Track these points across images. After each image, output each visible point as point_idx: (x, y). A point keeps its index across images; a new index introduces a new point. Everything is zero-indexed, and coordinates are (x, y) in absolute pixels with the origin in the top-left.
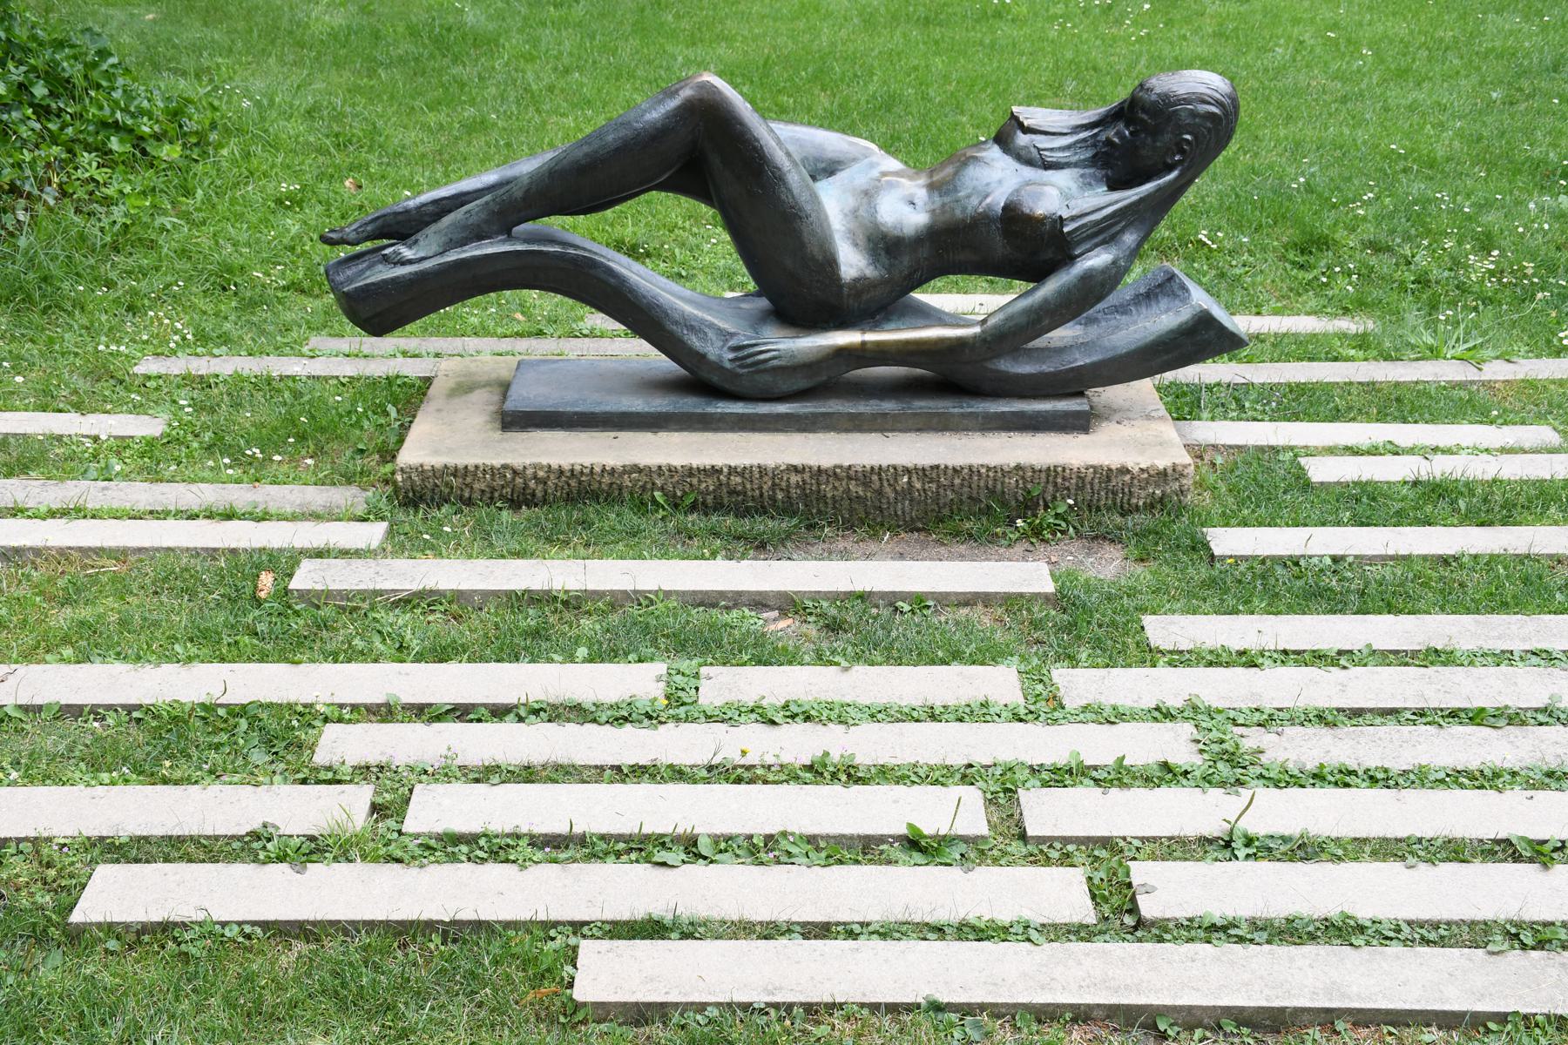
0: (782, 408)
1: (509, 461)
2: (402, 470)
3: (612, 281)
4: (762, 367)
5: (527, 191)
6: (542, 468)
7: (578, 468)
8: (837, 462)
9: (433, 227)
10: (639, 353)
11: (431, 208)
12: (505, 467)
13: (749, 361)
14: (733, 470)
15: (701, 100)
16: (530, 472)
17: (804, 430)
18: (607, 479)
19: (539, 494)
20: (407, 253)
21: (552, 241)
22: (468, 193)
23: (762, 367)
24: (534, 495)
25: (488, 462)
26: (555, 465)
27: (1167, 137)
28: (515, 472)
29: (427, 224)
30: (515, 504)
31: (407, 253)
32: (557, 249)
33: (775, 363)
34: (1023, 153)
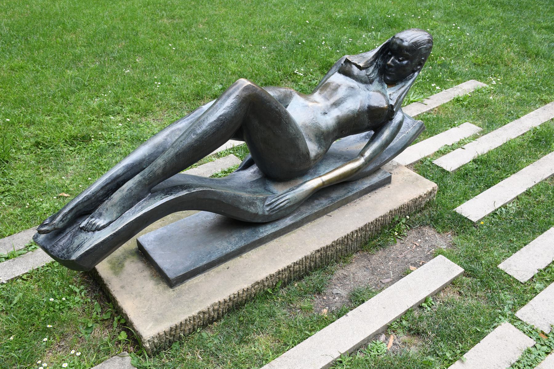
0: (288, 221)
1: (200, 309)
2: (149, 341)
3: (215, 198)
4: (282, 208)
5: (164, 169)
6: (216, 304)
7: (232, 296)
8: (333, 240)
9: (108, 204)
10: (205, 217)
11: (102, 192)
12: (199, 313)
13: (277, 207)
14: (295, 264)
15: (249, 96)
16: (211, 309)
17: (299, 227)
18: (245, 294)
19: (216, 316)
20: (101, 222)
21: (182, 187)
22: (118, 177)
23: (282, 208)
24: (213, 318)
25: (191, 315)
26: (222, 301)
27: (417, 60)
28: (204, 313)
29: (102, 201)
30: (204, 326)
31: (101, 222)
32: (184, 193)
33: (288, 205)
34: (363, 79)
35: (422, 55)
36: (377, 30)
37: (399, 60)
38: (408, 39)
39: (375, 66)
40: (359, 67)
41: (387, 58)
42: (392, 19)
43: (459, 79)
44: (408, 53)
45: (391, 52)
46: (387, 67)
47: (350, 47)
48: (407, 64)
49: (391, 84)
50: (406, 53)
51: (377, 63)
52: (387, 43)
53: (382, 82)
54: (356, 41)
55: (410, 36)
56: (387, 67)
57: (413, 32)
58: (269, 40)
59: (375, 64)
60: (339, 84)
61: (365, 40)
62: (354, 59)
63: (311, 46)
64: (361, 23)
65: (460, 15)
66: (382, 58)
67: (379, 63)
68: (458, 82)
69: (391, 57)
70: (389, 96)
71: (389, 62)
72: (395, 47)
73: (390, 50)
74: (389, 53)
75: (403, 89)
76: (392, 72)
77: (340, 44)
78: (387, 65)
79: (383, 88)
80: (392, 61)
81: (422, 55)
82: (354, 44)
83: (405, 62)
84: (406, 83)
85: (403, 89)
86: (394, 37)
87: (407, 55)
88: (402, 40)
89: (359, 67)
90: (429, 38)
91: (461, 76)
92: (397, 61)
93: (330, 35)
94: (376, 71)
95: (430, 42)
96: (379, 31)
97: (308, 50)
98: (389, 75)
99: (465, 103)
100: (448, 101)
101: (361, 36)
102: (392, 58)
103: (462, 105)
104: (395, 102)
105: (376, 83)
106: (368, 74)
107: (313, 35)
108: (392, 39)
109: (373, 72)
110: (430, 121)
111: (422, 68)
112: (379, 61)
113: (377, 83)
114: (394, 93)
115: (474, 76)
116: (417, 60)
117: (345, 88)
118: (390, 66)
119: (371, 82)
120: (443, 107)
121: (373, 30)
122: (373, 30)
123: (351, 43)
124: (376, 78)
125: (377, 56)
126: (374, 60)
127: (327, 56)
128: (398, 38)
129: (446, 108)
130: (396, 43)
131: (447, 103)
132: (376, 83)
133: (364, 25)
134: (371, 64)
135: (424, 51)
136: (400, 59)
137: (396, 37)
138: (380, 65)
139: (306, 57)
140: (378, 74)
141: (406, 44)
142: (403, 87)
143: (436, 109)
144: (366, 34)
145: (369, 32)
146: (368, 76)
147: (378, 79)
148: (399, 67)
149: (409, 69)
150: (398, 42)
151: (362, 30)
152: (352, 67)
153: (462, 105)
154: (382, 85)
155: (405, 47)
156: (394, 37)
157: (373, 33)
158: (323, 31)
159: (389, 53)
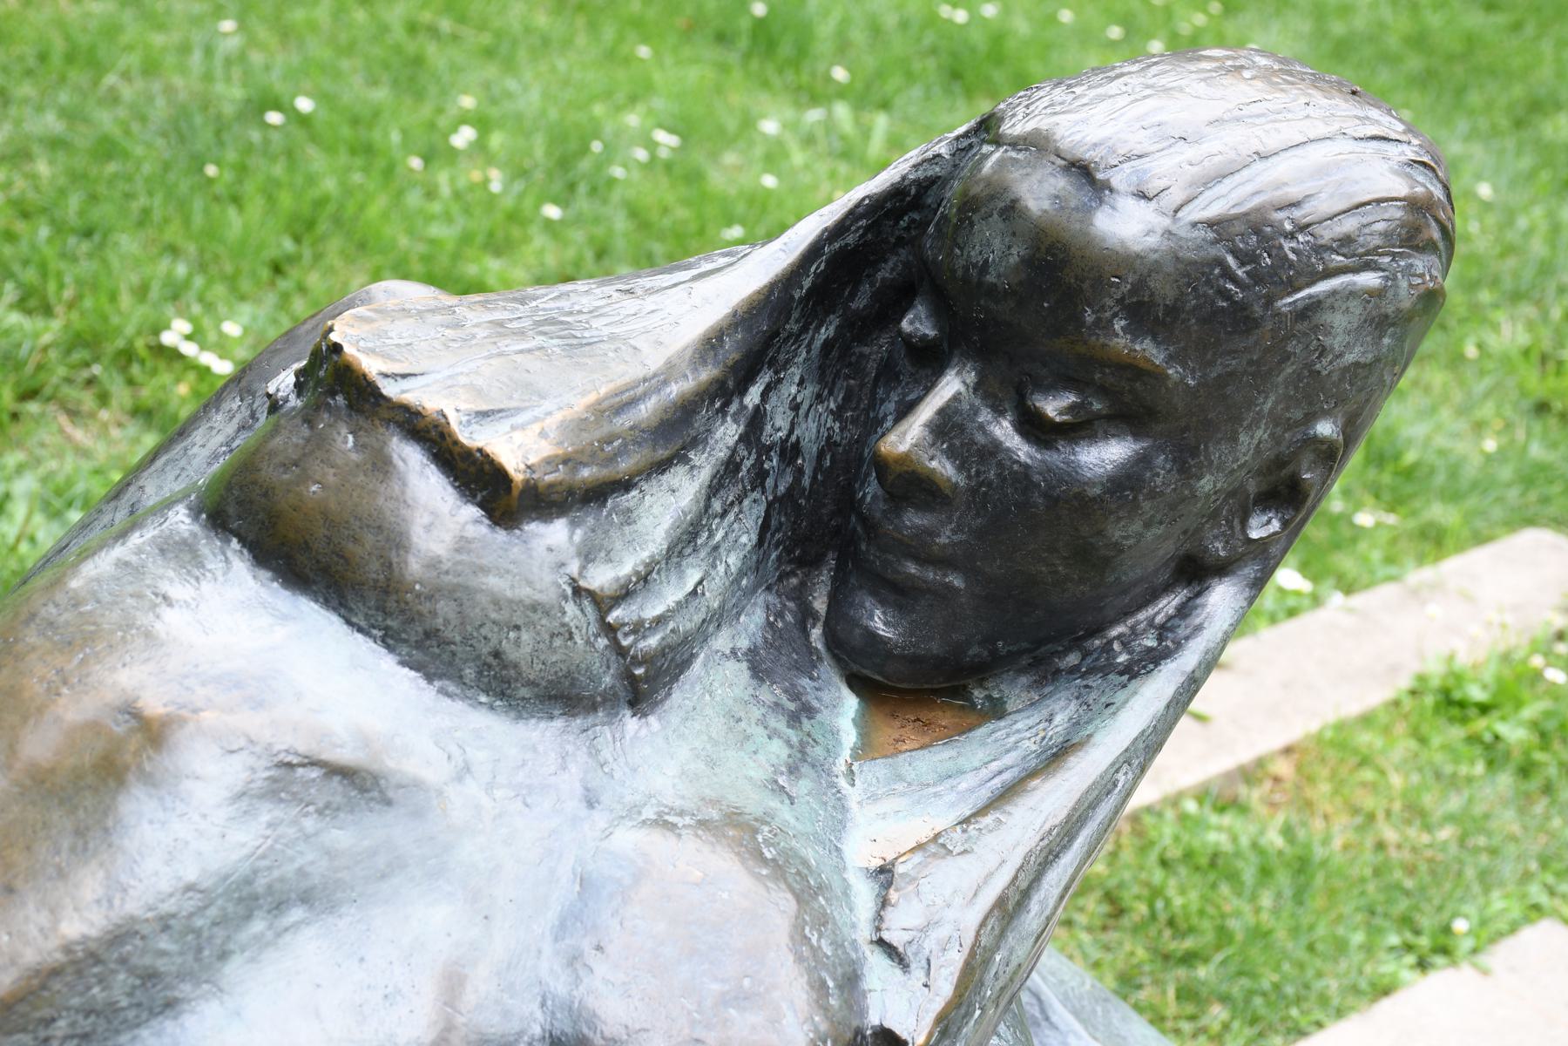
27: (1252, 442)
34: (522, 648)
35: (1313, 392)
36: (866, 97)
37: (1034, 427)
38: (1170, 169)
39: (730, 467)
40: (477, 477)
41: (888, 374)
42: (978, 38)
43: (1440, 513)
44: (1150, 351)
45: (942, 310)
46: (871, 489)
47: (659, 193)
48: (1125, 482)
49: (921, 688)
50: (1121, 341)
51: (756, 420)
52: (897, 193)
53: (807, 663)
54: (714, 156)
55: (1179, 145)
56: (871, 489)
57: (1239, 91)
58: (43, 57)
59: (728, 433)
60: (154, 704)
61: (774, 157)
62: (402, 338)
63: (365, 150)
64: (764, 38)
65: (1415, 63)
66: (831, 368)
67: (779, 423)
68: (1434, 542)
69: (928, 361)
70: (864, 895)
71: (906, 438)
72: (994, 250)
73: (915, 281)
74: (917, 323)
75: (1053, 798)
76: (926, 559)
77: (585, 165)
78: (881, 465)
79: (801, 760)
80: (947, 427)
81: (1313, 392)
82: (694, 177)
83: (1105, 455)
84: (1097, 710)
85: (1053, 798)
86: (987, 128)
87: (1135, 371)
88: (1082, 171)
89: (477, 477)
90: (1426, 186)
91: (1452, 495)
92: (1004, 432)
93: (529, 92)
94: (739, 534)
95: (1424, 227)
96: (885, 105)
97: (327, 175)
98: (899, 594)
99: (1514, 733)
100: (1375, 697)
101: (748, 123)
102: (950, 386)
103: (1494, 753)
104: (945, 987)
105: (718, 684)
106: (601, 578)
107: (410, 75)
108: (963, 149)
109: (687, 539)
110: (1233, 877)
111: (1291, 531)
112: (791, 405)
113: (737, 672)
114: (933, 847)
115: (1545, 500)
116: (1252, 442)
117: (236, 771)
118: (910, 486)
119: (642, 684)
120: (1336, 752)
121: (842, 92)
122: (842, 92)
123: (668, 167)
124: (718, 618)
125: (757, 342)
126: (723, 392)
127: (466, 239)
128: (1038, 144)
129: (1364, 762)
130: (1012, 210)
131: (1366, 720)
132: (718, 684)
133: (785, 49)
134: (675, 434)
135: (1343, 337)
136: (1053, 407)
137: (1015, 127)
138: (789, 451)
139: (302, 227)
140: (756, 564)
141: (1126, 225)
142: (1056, 755)
143: (1283, 768)
144: (789, 113)
145: (815, 99)
146: (602, 603)
147: (753, 622)
148: (1012, 508)
149: (1145, 540)
150: (1039, 192)
151: (765, 84)
152: (382, 466)
153: (1494, 753)
154: (801, 712)
155: (1125, 262)
156: (987, 128)
157: (842, 111)
158: (489, 53)
159: (917, 323)
